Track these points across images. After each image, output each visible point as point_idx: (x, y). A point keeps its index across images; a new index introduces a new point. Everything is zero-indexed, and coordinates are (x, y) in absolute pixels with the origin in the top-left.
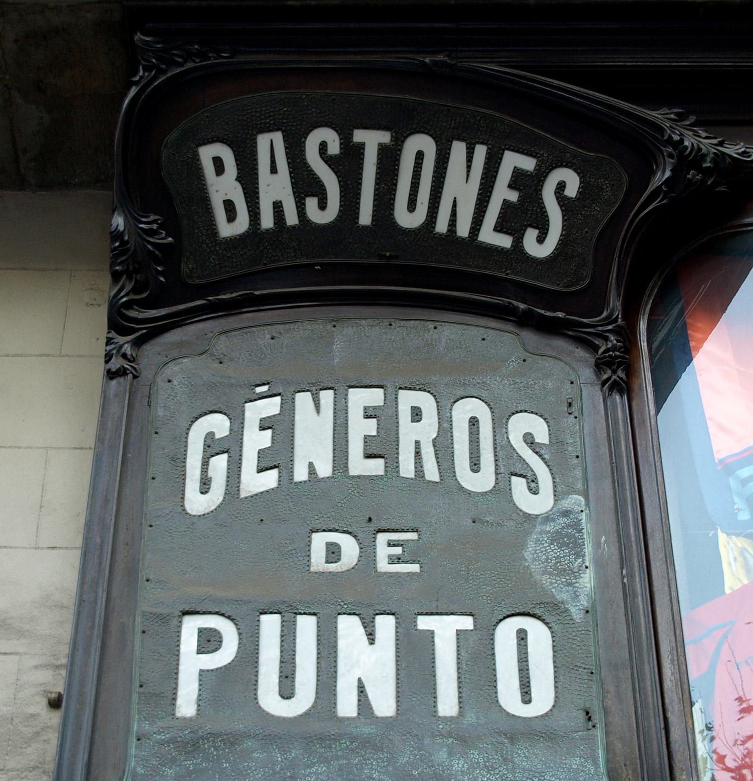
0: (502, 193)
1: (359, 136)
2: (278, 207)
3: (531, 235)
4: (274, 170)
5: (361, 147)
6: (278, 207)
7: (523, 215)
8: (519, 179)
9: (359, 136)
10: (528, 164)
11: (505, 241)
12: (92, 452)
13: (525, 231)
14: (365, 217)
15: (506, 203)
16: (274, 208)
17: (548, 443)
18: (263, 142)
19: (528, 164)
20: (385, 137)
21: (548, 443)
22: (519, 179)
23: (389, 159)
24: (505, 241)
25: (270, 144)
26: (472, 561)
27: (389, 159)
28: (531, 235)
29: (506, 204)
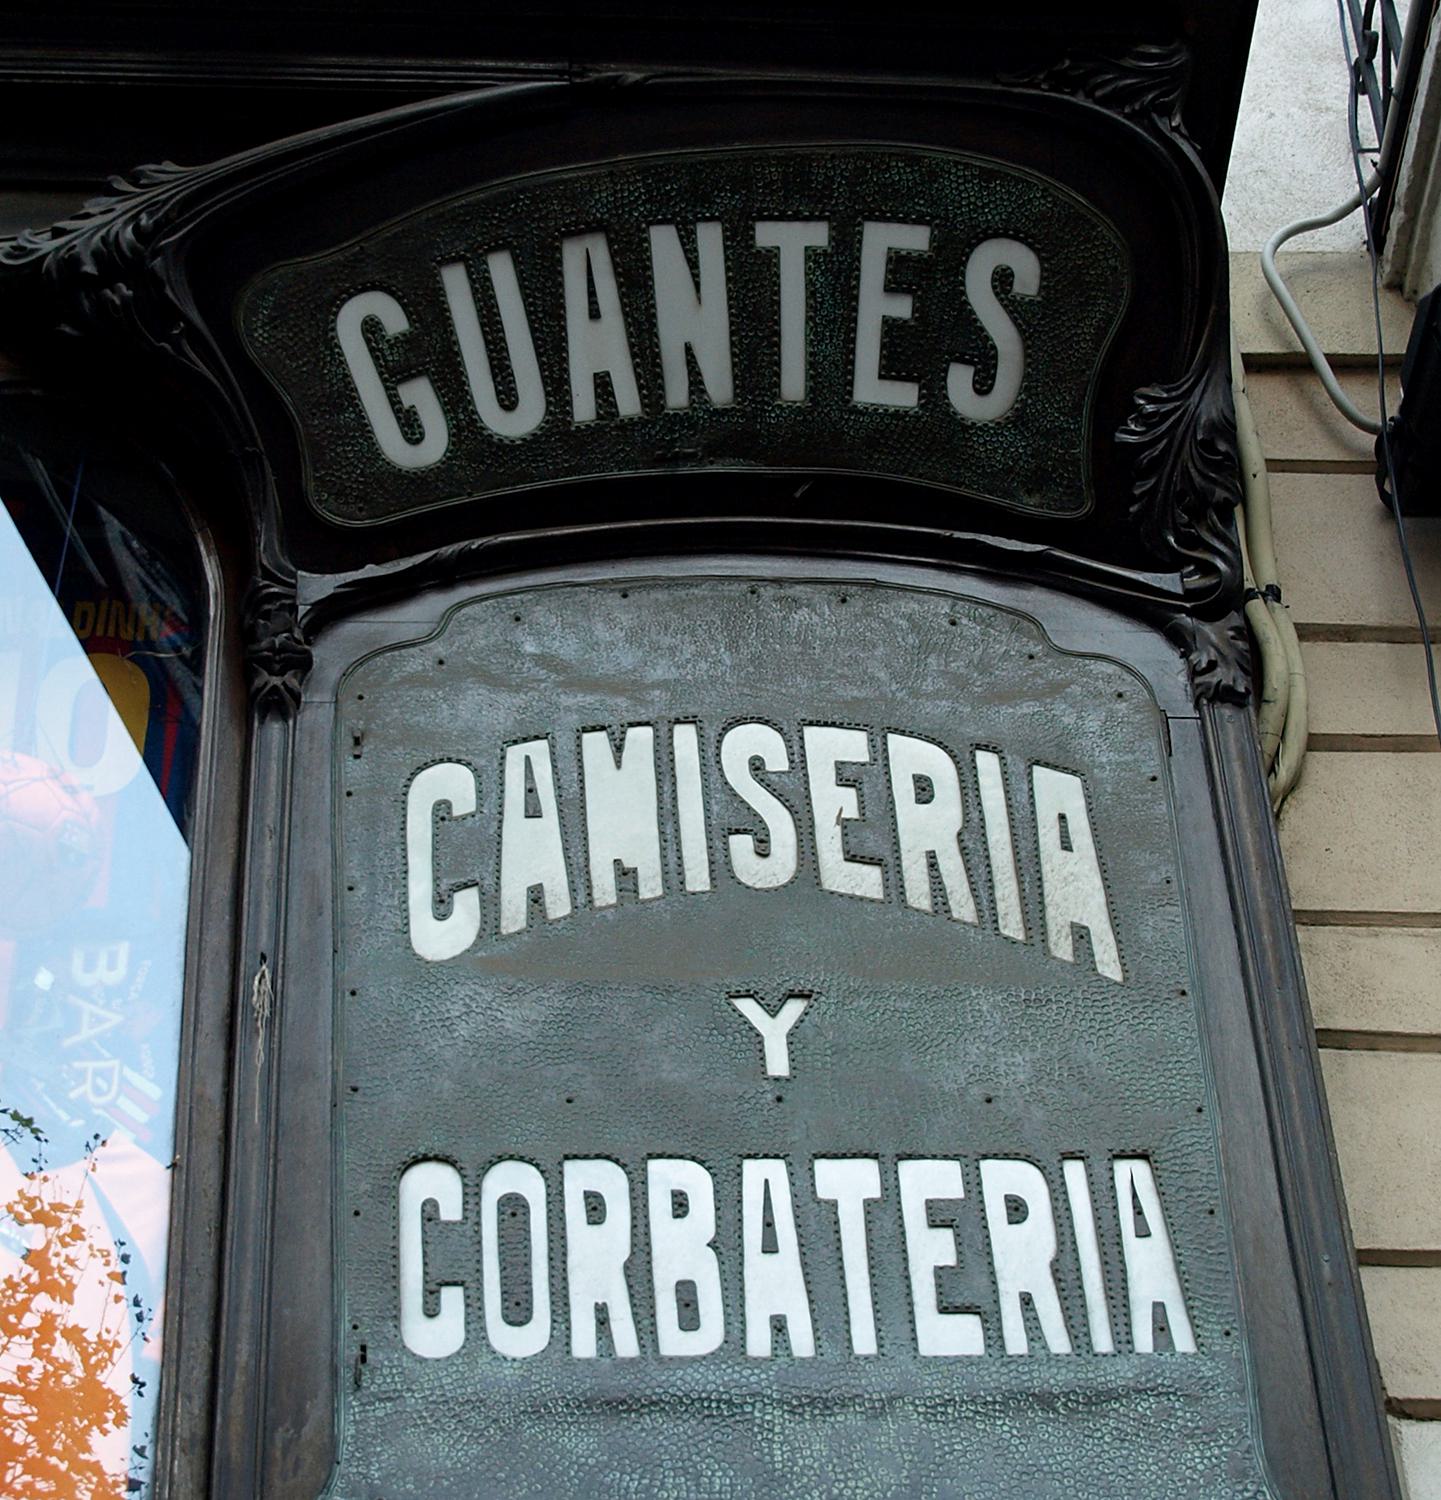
0: (878, 306)
1: (766, 234)
2: (603, 385)
3: (959, 380)
4: (595, 314)
5: (771, 257)
6: (603, 385)
7: (933, 339)
8: (902, 272)
9: (766, 234)
10: (915, 239)
11: (904, 396)
12: (1376, 351)
13: (946, 371)
14: (793, 383)
15: (890, 326)
16: (597, 386)
17: (880, 896)
18: (573, 256)
19: (915, 239)
20: (817, 234)
21: (880, 896)
22: (902, 272)
23: (835, 277)
24: (904, 396)
25: (585, 261)
26: (896, 1030)
27: (835, 277)
28: (959, 380)
29: (890, 326)
